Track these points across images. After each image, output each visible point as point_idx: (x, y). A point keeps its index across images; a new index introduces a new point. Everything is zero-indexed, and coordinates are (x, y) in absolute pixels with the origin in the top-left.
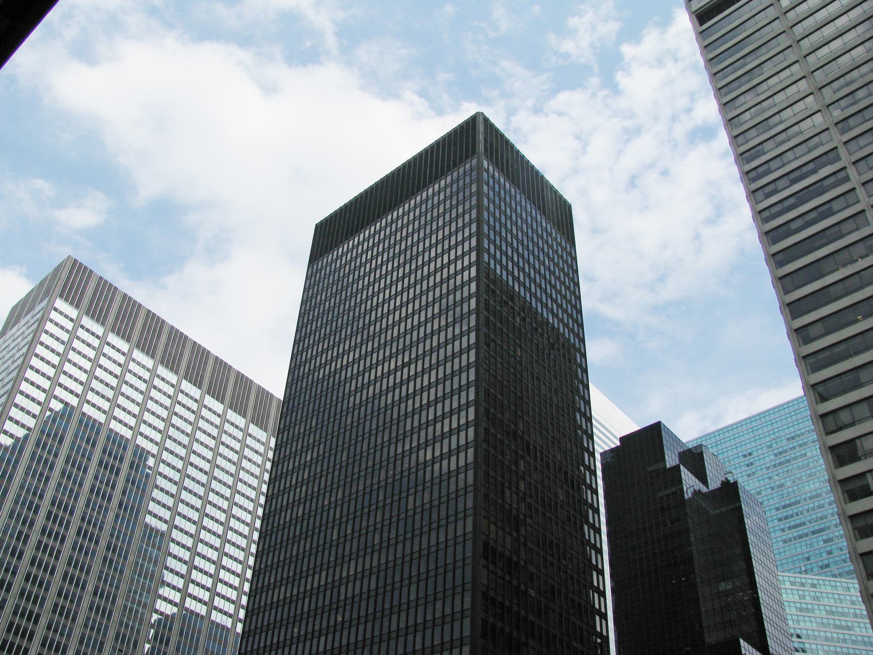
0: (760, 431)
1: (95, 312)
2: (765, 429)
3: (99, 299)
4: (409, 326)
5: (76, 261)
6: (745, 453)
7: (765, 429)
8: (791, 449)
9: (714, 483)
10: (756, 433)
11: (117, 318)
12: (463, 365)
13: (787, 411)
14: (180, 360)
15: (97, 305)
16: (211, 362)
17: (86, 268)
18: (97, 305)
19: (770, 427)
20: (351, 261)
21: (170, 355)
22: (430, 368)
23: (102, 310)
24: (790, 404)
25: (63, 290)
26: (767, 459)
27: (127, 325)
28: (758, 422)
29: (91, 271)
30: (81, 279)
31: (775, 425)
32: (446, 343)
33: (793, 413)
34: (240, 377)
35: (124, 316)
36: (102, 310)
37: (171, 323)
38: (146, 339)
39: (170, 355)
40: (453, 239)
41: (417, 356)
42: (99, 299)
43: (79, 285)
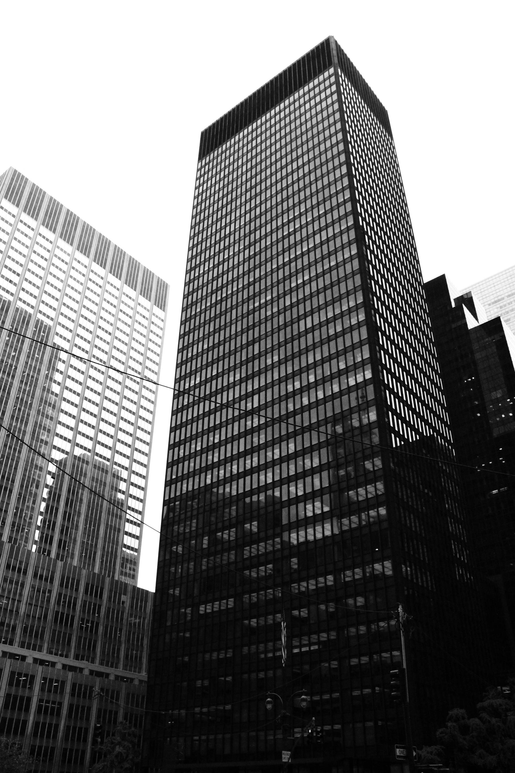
0: (486, 292)
1: (30, 210)
2: (490, 290)
3: (33, 201)
4: (236, 262)
5: (15, 171)
6: (489, 302)
7: (490, 290)
8: (509, 304)
9: (484, 319)
10: (497, 287)
11: (46, 215)
12: (244, 327)
13: (505, 276)
14: (90, 247)
15: (32, 205)
16: (112, 249)
17: (23, 177)
18: (32, 205)
19: (493, 289)
20: (205, 209)
21: (83, 244)
22: (255, 268)
23: (35, 208)
24: (507, 271)
25: (7, 193)
26: (492, 312)
27: (53, 220)
28: (485, 285)
29: (27, 179)
30: (20, 185)
31: (497, 287)
32: (277, 216)
33: (509, 278)
34: (132, 261)
35: (51, 214)
36: (35, 208)
37: (84, 220)
38: (67, 231)
39: (83, 244)
40: (268, 181)
41: (232, 306)
42: (33, 201)
43: (19, 189)
